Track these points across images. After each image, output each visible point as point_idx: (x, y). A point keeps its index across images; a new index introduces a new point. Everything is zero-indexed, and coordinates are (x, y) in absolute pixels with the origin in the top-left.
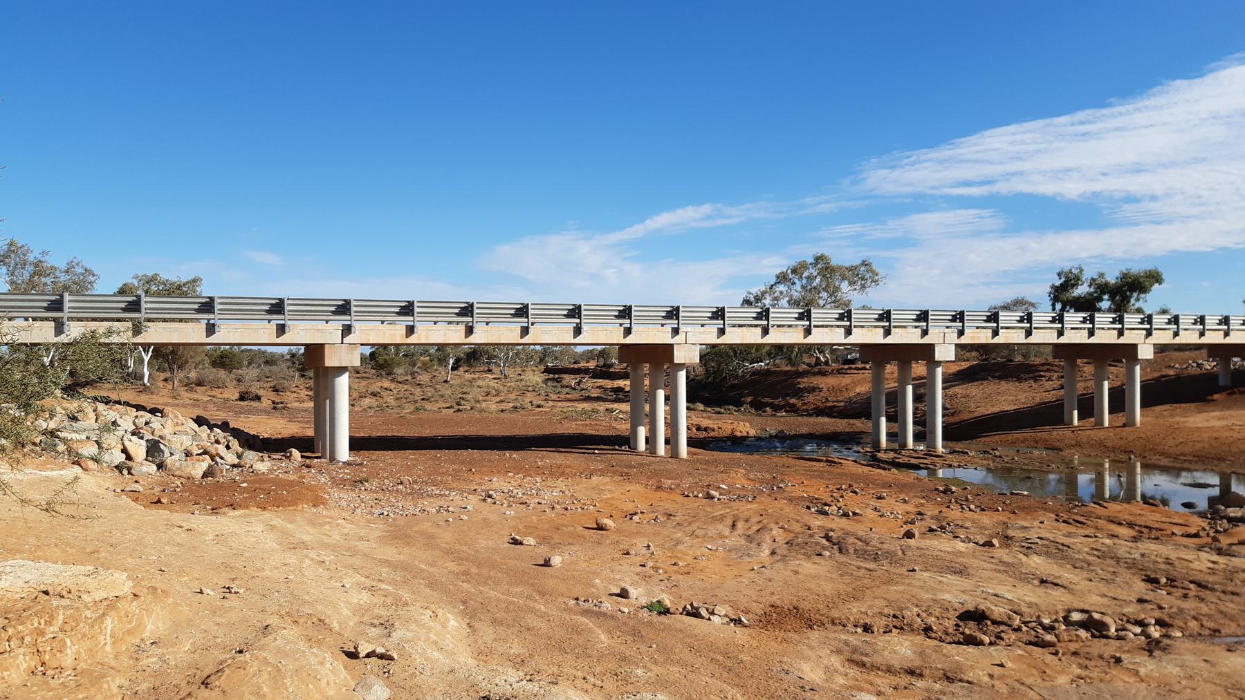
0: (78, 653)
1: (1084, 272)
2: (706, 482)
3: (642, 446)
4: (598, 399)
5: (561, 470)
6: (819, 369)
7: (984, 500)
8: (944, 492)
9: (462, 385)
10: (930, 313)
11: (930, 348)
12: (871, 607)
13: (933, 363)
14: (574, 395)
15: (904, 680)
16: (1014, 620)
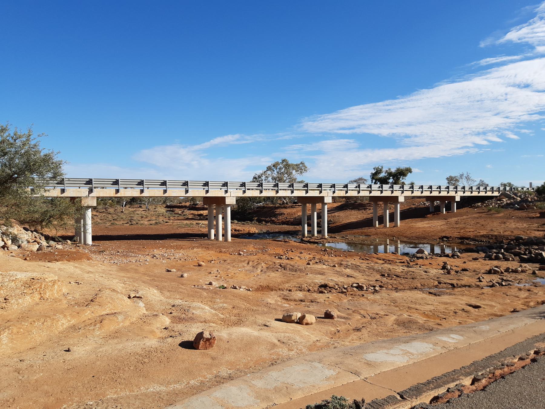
0: (49, 295)
1: (383, 168)
2: (238, 249)
3: (213, 237)
4: (192, 219)
5: (181, 247)
6: (284, 206)
7: (338, 253)
8: (324, 251)
9: (130, 213)
10: (323, 185)
11: (323, 198)
12: (292, 285)
13: (324, 204)
14: (181, 217)
15: (299, 302)
16: (336, 286)
